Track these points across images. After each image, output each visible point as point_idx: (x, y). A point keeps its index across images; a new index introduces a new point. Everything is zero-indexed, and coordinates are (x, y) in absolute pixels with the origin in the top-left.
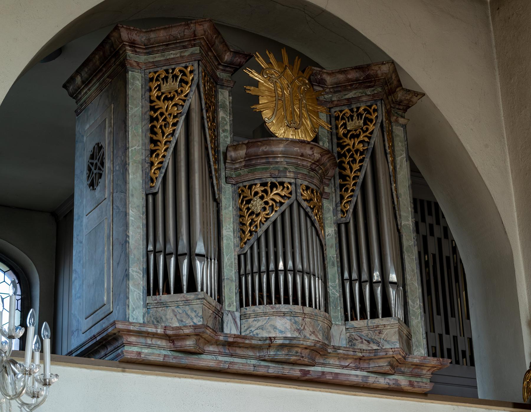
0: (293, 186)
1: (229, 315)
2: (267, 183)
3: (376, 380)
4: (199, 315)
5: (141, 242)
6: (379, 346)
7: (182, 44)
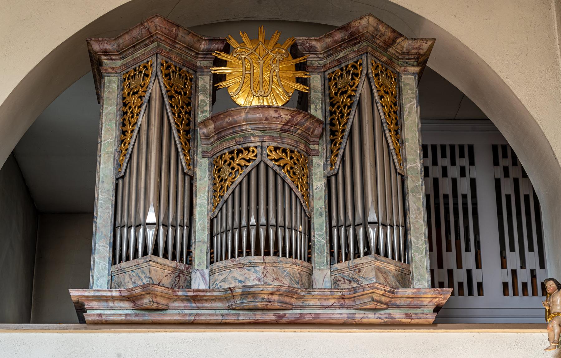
0: (259, 149)
1: (198, 272)
2: (234, 150)
3: (365, 316)
4: (147, 275)
5: (109, 221)
6: (358, 284)
7: (144, 43)
